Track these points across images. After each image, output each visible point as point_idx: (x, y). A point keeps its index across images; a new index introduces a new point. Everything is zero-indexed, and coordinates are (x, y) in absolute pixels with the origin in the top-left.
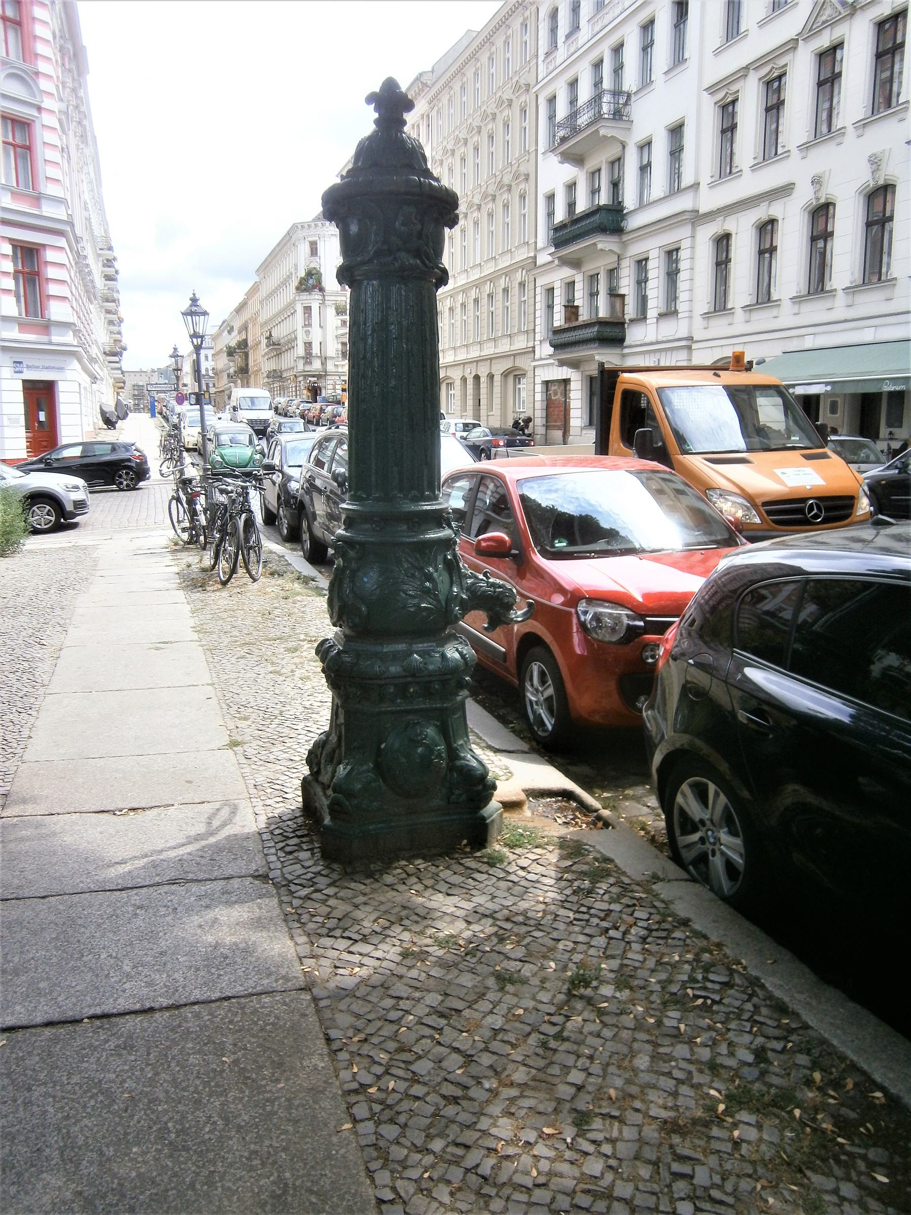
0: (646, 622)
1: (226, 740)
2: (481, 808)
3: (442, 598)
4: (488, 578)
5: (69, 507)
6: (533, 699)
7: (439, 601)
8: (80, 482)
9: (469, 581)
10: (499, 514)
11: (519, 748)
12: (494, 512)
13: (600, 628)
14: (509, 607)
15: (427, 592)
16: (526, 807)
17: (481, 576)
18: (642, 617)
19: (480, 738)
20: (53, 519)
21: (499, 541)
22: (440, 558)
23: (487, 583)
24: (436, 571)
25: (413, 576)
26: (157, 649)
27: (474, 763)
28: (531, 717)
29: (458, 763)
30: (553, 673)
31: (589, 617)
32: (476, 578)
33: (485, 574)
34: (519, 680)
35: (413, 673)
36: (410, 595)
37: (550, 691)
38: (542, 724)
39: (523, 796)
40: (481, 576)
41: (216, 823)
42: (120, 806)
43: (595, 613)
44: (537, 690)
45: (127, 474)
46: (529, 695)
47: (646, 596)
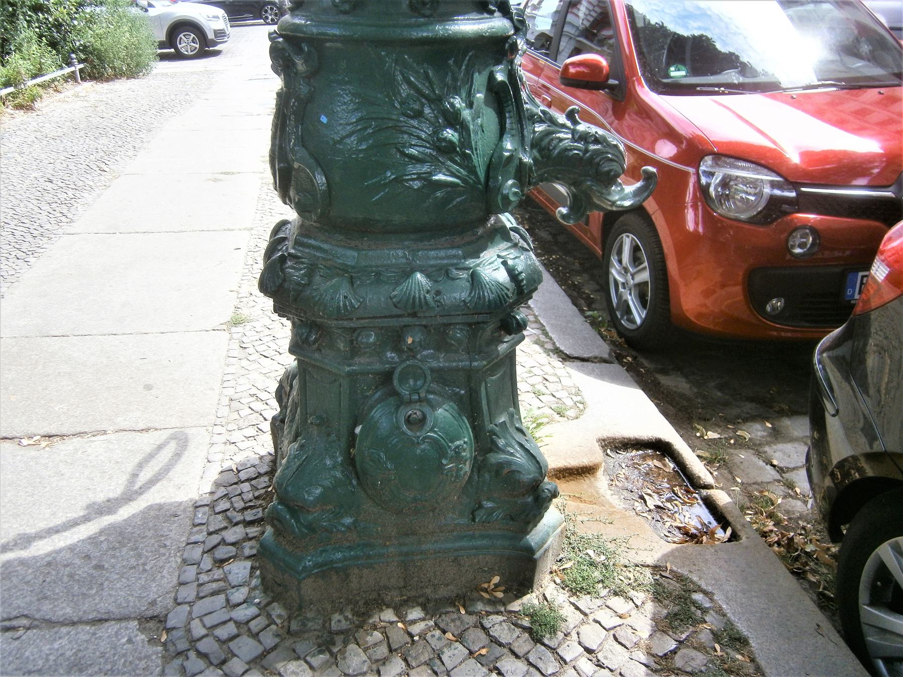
0: (800, 194)
1: (228, 315)
2: (525, 531)
3: (480, 162)
4: (575, 123)
5: (211, 36)
6: (620, 279)
7: (472, 170)
8: (220, 12)
9: (539, 128)
10: (592, 41)
11: (596, 353)
12: (586, 38)
14: (609, 179)
15: (447, 150)
16: (600, 473)
17: (562, 119)
18: (794, 185)
19: (546, 334)
20: (198, 46)
21: (594, 67)
22: (480, 79)
23: (574, 132)
24: (470, 105)
25: (419, 115)
26: (215, 180)
27: (520, 458)
28: (615, 300)
31: (716, 180)
32: (552, 121)
33: (571, 116)
34: (603, 250)
35: (414, 308)
36: (411, 157)
37: (645, 276)
38: (628, 311)
40: (562, 119)
41: (145, 476)
42: (32, 430)
44: (626, 270)
45: (272, 9)
46: (613, 271)
47: (807, 155)
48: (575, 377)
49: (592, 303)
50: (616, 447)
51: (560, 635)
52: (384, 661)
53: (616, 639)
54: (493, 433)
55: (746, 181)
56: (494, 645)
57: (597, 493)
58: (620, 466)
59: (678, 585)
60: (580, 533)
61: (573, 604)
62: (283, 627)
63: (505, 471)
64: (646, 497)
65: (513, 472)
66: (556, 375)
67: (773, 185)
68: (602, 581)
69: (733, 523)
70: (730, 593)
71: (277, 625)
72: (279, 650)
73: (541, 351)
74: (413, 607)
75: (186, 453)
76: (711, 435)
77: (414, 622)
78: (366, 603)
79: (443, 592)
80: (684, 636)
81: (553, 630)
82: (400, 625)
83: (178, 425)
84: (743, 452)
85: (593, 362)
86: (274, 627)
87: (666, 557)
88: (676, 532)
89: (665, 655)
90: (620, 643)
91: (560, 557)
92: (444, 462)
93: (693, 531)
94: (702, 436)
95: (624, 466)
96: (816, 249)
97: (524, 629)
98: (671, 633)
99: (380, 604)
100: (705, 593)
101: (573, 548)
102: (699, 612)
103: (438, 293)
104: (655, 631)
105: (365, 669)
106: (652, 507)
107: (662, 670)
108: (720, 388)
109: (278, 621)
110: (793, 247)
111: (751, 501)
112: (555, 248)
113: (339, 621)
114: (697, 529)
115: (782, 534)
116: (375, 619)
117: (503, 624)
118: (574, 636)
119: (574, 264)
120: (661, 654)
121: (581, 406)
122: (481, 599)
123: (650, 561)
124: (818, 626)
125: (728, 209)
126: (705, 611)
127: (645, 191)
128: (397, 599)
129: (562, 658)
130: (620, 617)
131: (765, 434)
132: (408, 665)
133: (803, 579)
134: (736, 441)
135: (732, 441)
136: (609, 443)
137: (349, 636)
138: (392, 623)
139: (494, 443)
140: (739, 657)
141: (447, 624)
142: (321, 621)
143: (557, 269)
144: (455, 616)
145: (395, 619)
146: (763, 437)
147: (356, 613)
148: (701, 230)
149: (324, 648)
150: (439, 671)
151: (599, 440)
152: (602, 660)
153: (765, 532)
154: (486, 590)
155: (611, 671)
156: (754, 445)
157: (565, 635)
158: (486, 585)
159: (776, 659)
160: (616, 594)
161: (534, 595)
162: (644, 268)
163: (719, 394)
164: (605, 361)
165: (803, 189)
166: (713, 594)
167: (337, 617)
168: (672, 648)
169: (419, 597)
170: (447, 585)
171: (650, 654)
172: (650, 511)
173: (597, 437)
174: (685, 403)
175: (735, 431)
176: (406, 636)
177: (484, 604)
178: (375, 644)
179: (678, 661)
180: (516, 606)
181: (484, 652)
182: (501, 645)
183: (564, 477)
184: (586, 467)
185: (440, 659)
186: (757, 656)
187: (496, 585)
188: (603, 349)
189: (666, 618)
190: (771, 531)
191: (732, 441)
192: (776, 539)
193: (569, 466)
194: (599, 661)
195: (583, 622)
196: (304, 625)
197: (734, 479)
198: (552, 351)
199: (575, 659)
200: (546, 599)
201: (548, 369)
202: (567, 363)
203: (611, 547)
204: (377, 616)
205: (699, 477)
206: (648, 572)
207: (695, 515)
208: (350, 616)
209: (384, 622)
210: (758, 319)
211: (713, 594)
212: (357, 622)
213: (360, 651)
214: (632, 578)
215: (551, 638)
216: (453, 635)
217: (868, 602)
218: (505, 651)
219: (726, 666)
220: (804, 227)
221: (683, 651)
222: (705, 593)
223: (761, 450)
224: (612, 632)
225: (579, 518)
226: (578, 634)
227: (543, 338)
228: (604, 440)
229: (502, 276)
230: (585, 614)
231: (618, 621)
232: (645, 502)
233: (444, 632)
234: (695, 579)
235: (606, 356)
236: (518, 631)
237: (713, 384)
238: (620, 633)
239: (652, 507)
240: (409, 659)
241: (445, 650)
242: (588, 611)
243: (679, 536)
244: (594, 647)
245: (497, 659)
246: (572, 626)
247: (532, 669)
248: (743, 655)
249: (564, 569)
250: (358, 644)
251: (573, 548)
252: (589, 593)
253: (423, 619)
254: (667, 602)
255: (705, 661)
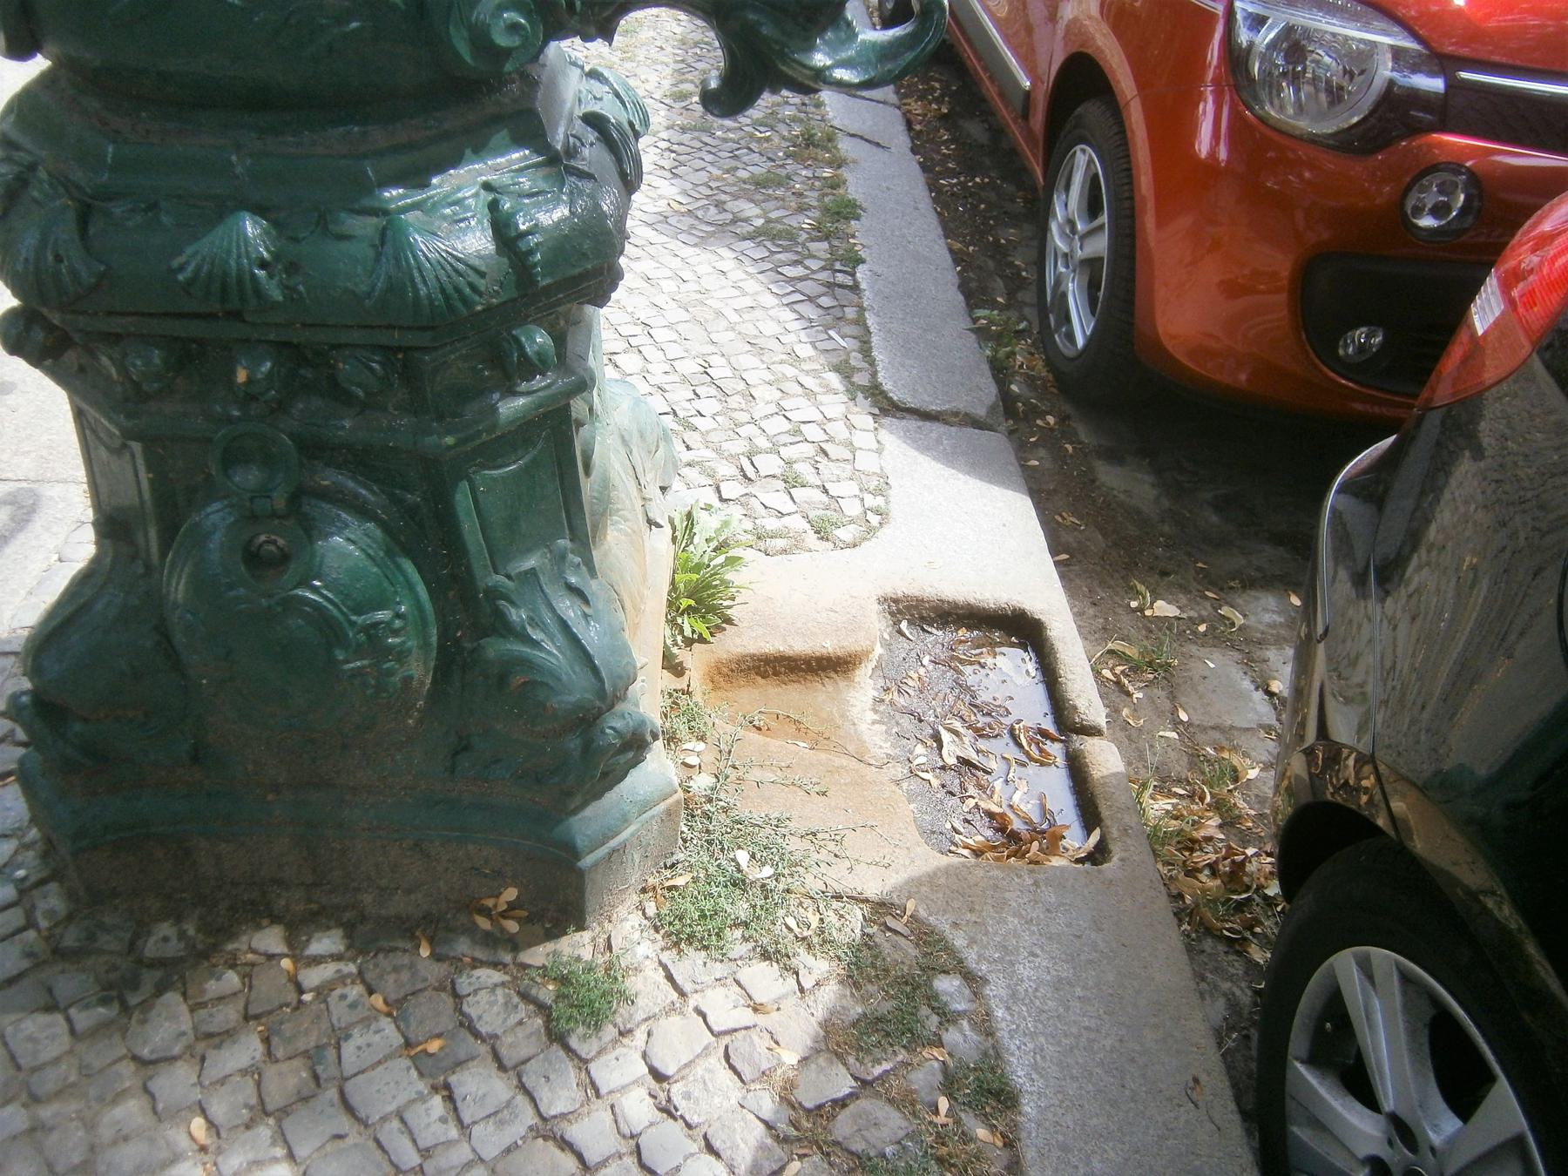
11: (962, 403)
13: (1295, 79)
16: (863, 673)
18: (1441, 62)
27: (552, 652)
29: (496, 648)
30: (1115, 200)
31: (1267, 36)
35: (228, 297)
37: (1100, 245)
39: (870, 631)
43: (1289, 30)
48: (895, 454)
49: (1020, 288)
50: (922, 618)
51: (609, 1032)
52: (225, 1037)
53: (727, 1057)
54: (494, 594)
55: (1339, 47)
56: (464, 1033)
57: (842, 716)
58: (919, 659)
59: (913, 952)
60: (743, 811)
61: (665, 968)
62: (47, 939)
63: (517, 680)
64: (946, 737)
65: (534, 683)
66: (849, 444)
67: (1397, 53)
68: (746, 925)
69: (1108, 822)
70: (1025, 985)
71: (39, 931)
72: (25, 982)
73: (841, 388)
74: (329, 928)
75: (21, 537)
76: (1163, 609)
77: (317, 960)
78: (232, 908)
79: (399, 905)
80: (877, 1071)
81: (595, 1018)
82: (286, 963)
83: (32, 475)
84: (1217, 654)
85: (946, 423)
86: (31, 934)
87: (914, 886)
88: (980, 822)
89: (820, 1107)
90: (732, 1067)
91: (674, 859)
92: (340, 655)
93: (1017, 825)
94: (1141, 609)
95: (926, 661)
96: (1470, 220)
97: (542, 1008)
98: (851, 1060)
99: (260, 912)
100: (969, 977)
101: (710, 842)
102: (935, 1019)
103: (293, 268)
104: (818, 1052)
105: (177, 1050)
106: (952, 761)
107: (799, 1140)
108: (1220, 506)
109: (44, 923)
110: (1418, 211)
111: (1192, 766)
112: (987, 162)
113: (166, 939)
114: (1028, 821)
115: (1229, 848)
116: (238, 945)
117: (499, 991)
118: (640, 1035)
119: (1013, 201)
120: (809, 1105)
121: (874, 520)
122: (471, 931)
123: (873, 890)
124: (1196, 1080)
125: (1286, 108)
126: (948, 1018)
127: (911, 48)
128: (300, 907)
129: (593, 1083)
130: (755, 1010)
131: (1280, 619)
132: (269, 1053)
133: (1239, 953)
134: (1212, 628)
135: (1202, 628)
136: (908, 608)
137: (174, 974)
138: (271, 957)
139: (500, 615)
140: (982, 1133)
141: (381, 977)
142: (129, 935)
143: (975, 207)
144: (406, 959)
145: (280, 948)
146: (1272, 626)
147: (205, 927)
148: (1223, 154)
149: (114, 993)
150: (323, 1076)
151: (883, 600)
152: (677, 1100)
153: (1194, 841)
154: (486, 912)
155: (689, 1126)
156: (1248, 641)
157: (621, 1034)
158: (490, 903)
159: (1064, 1148)
160: (766, 956)
161: (586, 936)
162: (1101, 227)
163: (1214, 519)
164: (977, 424)
165: (1464, 75)
166: (986, 981)
167: (166, 929)
168: (840, 1095)
169: (345, 909)
170: (409, 892)
171: (786, 1099)
172: (943, 768)
173: (881, 593)
174: (1133, 531)
175: (1217, 604)
176: (291, 987)
177: (474, 942)
178: (221, 999)
179: (843, 1126)
180: (537, 955)
181: (434, 1046)
182: (477, 1035)
183: (776, 674)
184: (829, 659)
185: (338, 1048)
186: (1023, 1135)
187: (512, 906)
188: (981, 394)
189: (854, 1025)
190: (1209, 839)
191: (1202, 628)
192: (1214, 857)
193: (791, 653)
194: (669, 1100)
195: (671, 1009)
196: (92, 937)
197: (1174, 712)
198: (863, 389)
199: (623, 1089)
200: (610, 947)
201: (839, 430)
202: (887, 421)
203: (795, 845)
204: (244, 938)
205: (1075, 708)
206: (856, 915)
207: (1036, 791)
208: (191, 932)
209: (254, 951)
210: (1316, 367)
211: (986, 981)
212: (200, 947)
213: (184, 1008)
214: (815, 924)
215: (585, 1038)
216: (386, 1002)
217: (1304, 1053)
218: (483, 1049)
219: (944, 1151)
220: (1456, 168)
221: (863, 1104)
222: (969, 977)
223: (1258, 654)
224: (726, 1040)
225: (756, 774)
226: (649, 1034)
227: (856, 360)
228: (896, 601)
229: (476, 242)
230: (682, 994)
231: (747, 1017)
232: (940, 747)
233: (371, 992)
234: (959, 941)
235: (981, 412)
236: (523, 1010)
237: (1208, 496)
238: (738, 1043)
239: (952, 761)
240: (275, 1040)
241: (356, 1032)
242: (688, 987)
243: (983, 834)
244: (669, 1070)
245: (459, 1064)
246: (640, 1016)
247: (521, 1100)
248: (992, 1128)
249: (670, 889)
250: (184, 995)
251: (710, 842)
252: (706, 948)
253: (337, 958)
254: (871, 988)
255: (901, 1133)
